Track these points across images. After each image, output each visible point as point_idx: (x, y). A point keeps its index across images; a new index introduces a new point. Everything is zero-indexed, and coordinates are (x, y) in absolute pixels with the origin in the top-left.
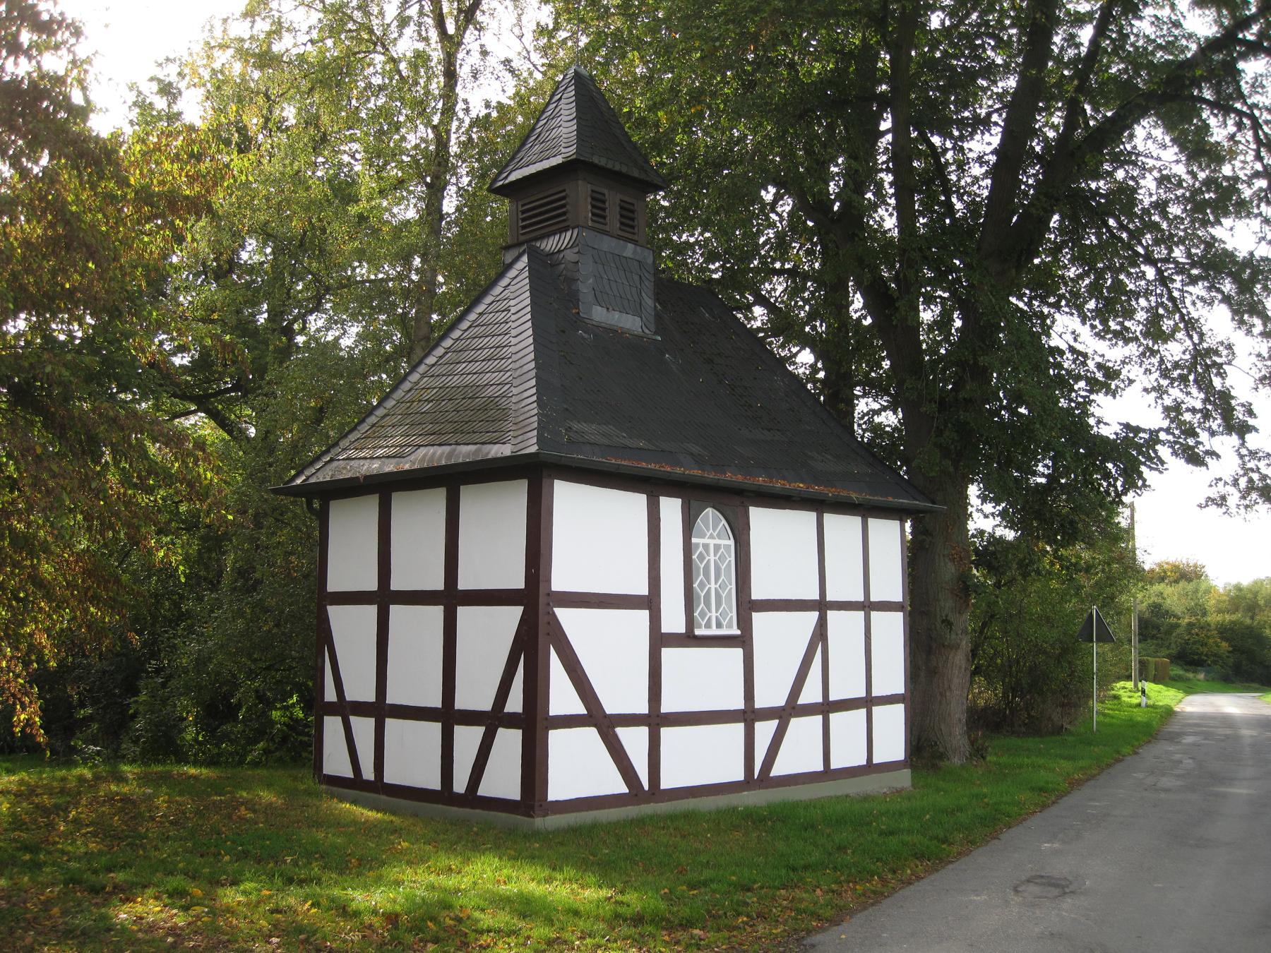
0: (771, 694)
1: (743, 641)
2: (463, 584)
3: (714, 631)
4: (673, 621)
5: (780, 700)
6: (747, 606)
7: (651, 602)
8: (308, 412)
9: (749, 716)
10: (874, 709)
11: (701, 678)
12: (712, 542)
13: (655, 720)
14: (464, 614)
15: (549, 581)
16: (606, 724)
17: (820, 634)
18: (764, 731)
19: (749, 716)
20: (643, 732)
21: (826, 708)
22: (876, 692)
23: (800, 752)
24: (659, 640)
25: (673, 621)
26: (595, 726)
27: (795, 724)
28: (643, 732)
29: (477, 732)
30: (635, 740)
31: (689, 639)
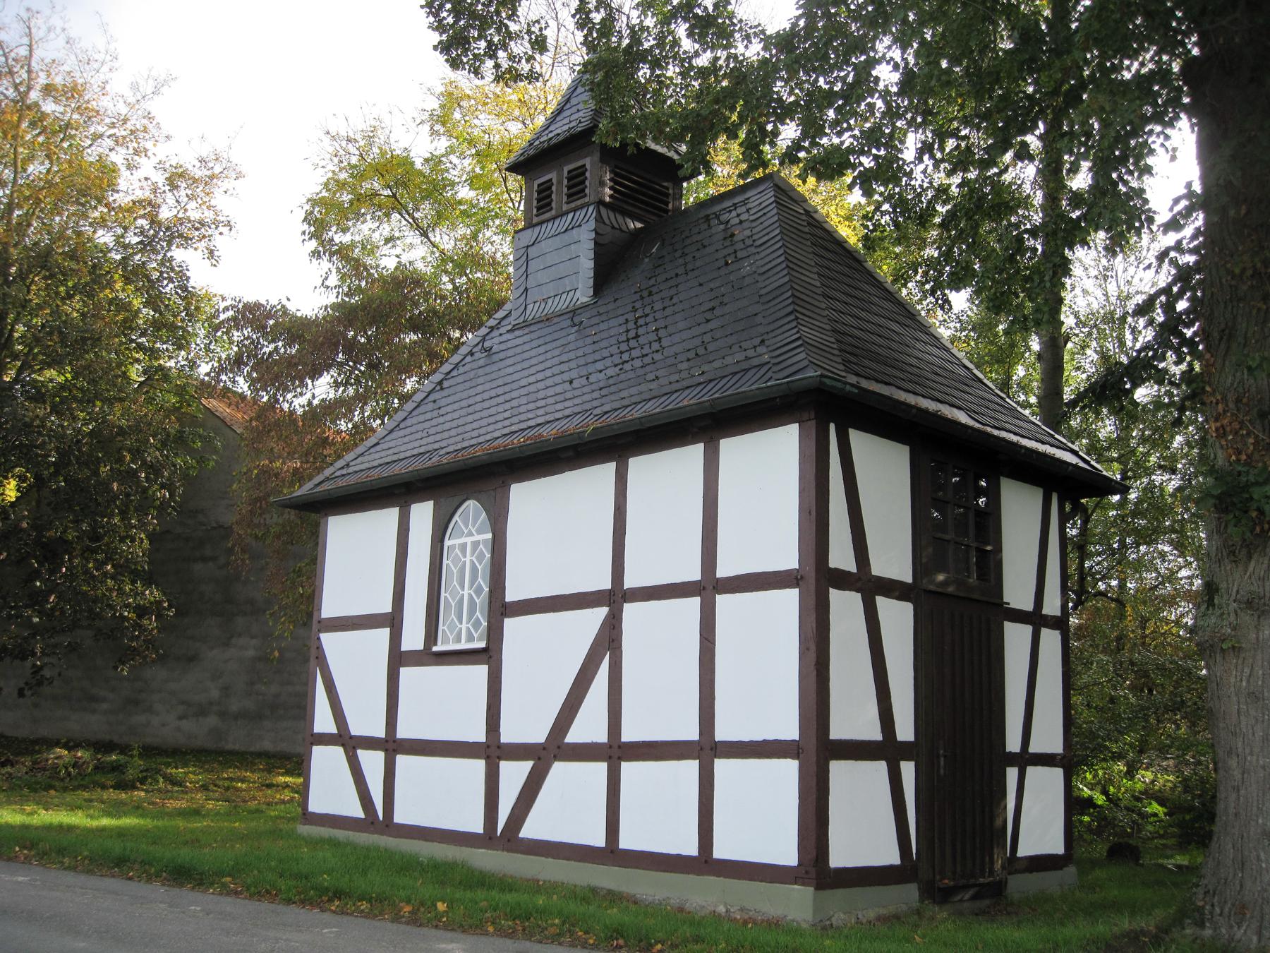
0: (526, 722)
1: (490, 655)
2: (722, 572)
3: (464, 645)
4: (413, 639)
5: (538, 734)
6: (500, 608)
7: (393, 621)
8: (994, 348)
9: (493, 751)
10: (625, 766)
11: (444, 702)
12: (469, 540)
13: (392, 746)
14: (724, 602)
15: (320, 610)
16: (350, 743)
17: (609, 640)
18: (514, 774)
19: (493, 751)
20: (379, 756)
21: (615, 752)
22: (629, 734)
23: (568, 809)
24: (398, 659)
25: (413, 639)
26: (343, 745)
27: (560, 771)
28: (379, 756)
29: (577, 734)
30: (372, 762)
31: (430, 656)
